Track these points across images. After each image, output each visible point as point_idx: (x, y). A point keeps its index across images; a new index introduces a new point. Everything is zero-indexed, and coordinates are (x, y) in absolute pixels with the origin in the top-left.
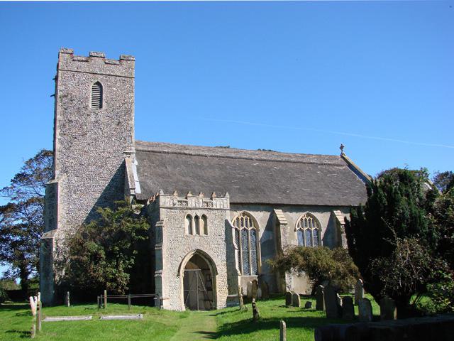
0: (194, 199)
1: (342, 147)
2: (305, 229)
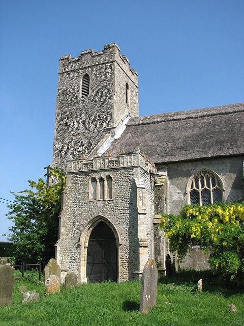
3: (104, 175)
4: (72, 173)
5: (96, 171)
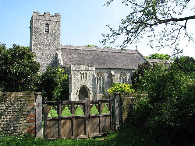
0: (83, 67)
1: (136, 47)
2: (121, 77)
3: (84, 72)
4: (73, 70)
5: (81, 71)
